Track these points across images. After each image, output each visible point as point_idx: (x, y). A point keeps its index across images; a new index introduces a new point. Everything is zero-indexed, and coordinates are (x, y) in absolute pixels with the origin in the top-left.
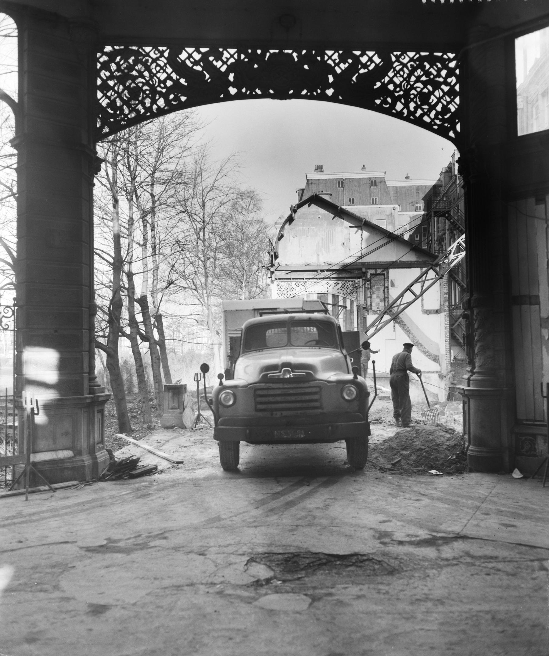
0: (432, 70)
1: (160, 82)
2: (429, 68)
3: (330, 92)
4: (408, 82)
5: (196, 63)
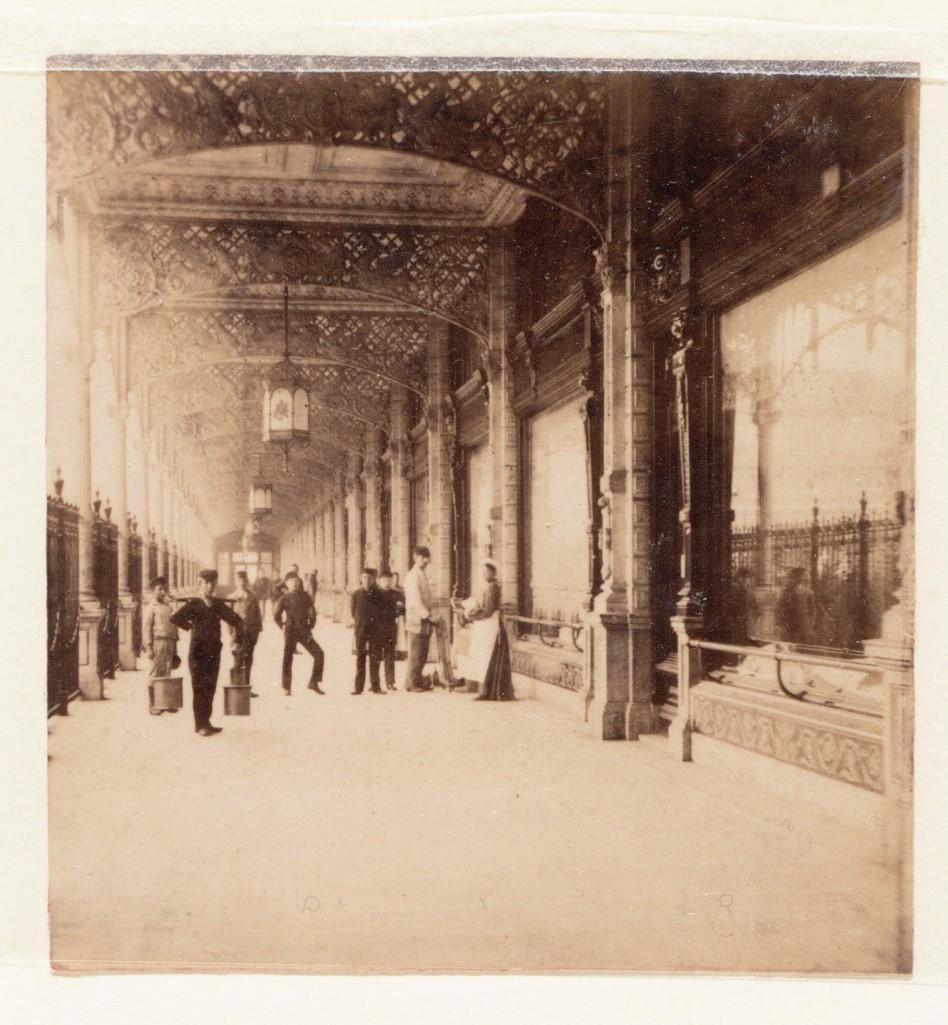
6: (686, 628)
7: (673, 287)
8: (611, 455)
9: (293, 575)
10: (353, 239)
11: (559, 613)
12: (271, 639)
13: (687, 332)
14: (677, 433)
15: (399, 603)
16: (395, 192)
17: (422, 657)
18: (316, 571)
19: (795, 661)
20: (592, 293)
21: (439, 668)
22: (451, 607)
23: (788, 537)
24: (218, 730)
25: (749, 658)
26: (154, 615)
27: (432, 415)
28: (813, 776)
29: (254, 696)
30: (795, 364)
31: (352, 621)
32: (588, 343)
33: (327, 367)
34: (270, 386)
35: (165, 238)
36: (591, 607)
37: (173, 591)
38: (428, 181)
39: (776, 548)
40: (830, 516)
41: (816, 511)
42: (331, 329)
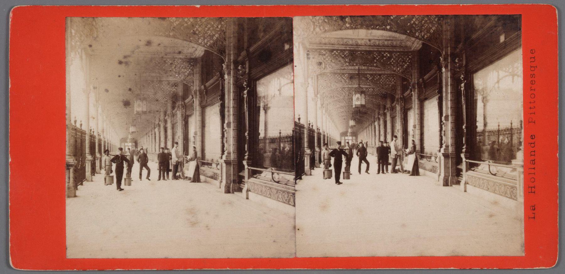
0: (404, 58)
6: (465, 157)
7: (460, 66)
8: (445, 111)
9: (361, 143)
10: (377, 54)
11: (431, 153)
12: (355, 160)
13: (248, 86)
14: (245, 112)
15: (389, 150)
16: (387, 42)
17: (395, 164)
18: (147, 148)
19: (494, 165)
20: (222, 76)
21: (400, 167)
22: (184, 158)
23: (273, 140)
24: (342, 183)
25: (481, 165)
26: (106, 159)
27: (398, 101)
28: (282, 203)
29: (351, 174)
30: (493, 87)
31: (377, 155)
32: (221, 88)
33: (370, 88)
34: (355, 93)
35: (327, 54)
36: (440, 151)
37: (329, 147)
38: (396, 39)
39: (489, 135)
40: (502, 127)
41: (499, 126)
42: (371, 78)
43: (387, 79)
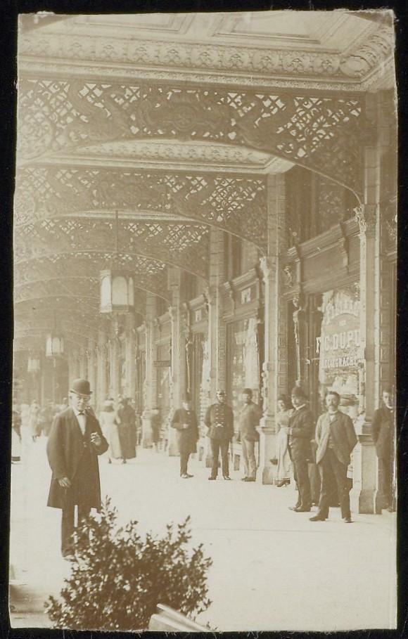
0: (245, 192)
1: (41, 195)
2: (332, 115)
3: (232, 135)
4: (311, 128)
5: (98, 99)
43: (151, 265)
